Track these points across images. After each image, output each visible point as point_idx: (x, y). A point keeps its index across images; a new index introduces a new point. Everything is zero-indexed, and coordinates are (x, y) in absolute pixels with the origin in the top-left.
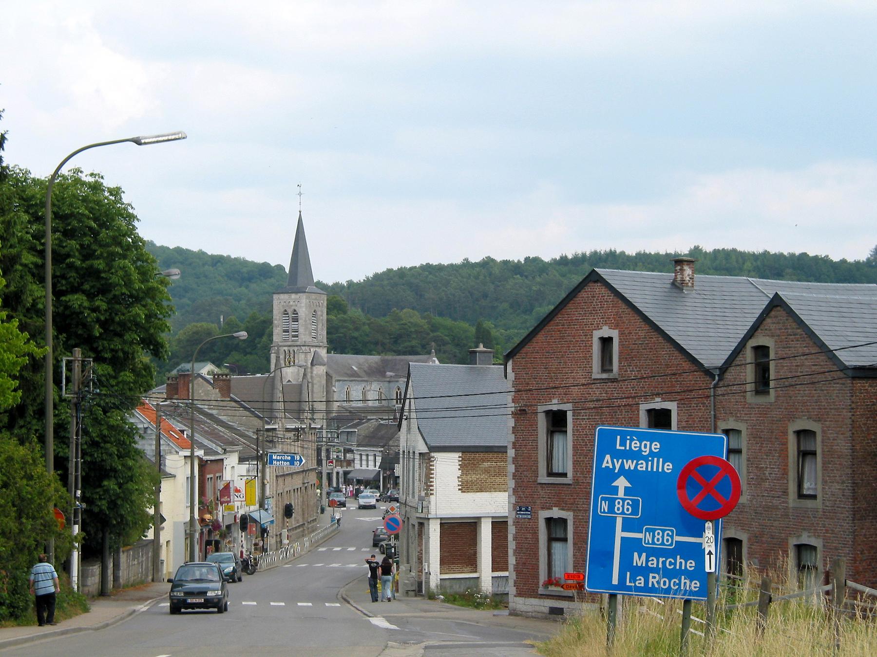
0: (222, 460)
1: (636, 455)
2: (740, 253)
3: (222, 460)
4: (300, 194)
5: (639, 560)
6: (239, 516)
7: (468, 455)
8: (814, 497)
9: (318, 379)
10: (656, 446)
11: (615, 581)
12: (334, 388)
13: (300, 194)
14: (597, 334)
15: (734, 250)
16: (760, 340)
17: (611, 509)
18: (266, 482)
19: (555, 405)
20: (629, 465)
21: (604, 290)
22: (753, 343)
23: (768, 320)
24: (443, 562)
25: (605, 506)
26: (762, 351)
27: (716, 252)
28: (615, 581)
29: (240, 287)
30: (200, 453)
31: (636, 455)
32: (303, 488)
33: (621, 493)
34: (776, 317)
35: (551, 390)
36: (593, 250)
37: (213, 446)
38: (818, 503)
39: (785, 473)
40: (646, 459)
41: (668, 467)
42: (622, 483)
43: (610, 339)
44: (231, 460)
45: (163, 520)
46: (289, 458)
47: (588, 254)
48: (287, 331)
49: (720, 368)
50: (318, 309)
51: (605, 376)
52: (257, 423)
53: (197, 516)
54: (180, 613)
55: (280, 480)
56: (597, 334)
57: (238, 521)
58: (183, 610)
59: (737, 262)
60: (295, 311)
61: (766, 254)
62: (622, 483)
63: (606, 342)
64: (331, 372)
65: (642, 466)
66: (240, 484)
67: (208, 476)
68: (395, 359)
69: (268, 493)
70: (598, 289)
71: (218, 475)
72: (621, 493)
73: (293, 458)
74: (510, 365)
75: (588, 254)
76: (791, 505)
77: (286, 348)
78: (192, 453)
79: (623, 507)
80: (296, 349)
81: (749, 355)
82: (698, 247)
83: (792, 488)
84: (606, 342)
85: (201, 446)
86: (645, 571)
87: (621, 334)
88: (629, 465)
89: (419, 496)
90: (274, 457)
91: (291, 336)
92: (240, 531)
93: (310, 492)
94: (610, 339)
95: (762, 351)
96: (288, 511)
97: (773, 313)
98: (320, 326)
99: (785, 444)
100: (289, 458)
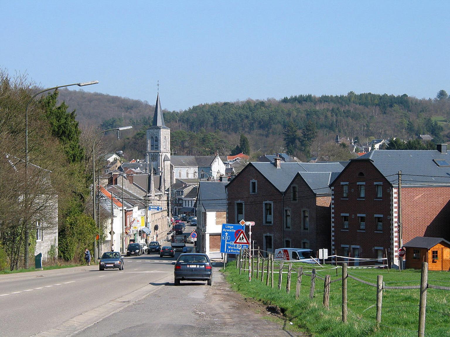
0: (132, 210)
1: (229, 229)
2: (373, 95)
3: (132, 210)
4: (158, 85)
5: (229, 247)
6: (138, 231)
7: (218, 213)
8: (307, 229)
9: (166, 167)
10: (233, 227)
11: (225, 251)
12: (173, 171)
13: (158, 85)
14: (251, 181)
15: (370, 94)
16: (294, 185)
17: (225, 238)
18: (148, 217)
19: (239, 201)
20: (228, 230)
21: (253, 168)
22: (292, 186)
23: (296, 180)
24: (210, 248)
25: (224, 238)
26: (294, 188)
27: (361, 95)
28: (225, 251)
29: (127, 112)
30: (125, 208)
31: (229, 229)
32: (162, 218)
33: (226, 235)
34: (298, 179)
35: (238, 199)
36: (300, 95)
37: (129, 205)
38: (308, 231)
39: (300, 222)
40: (231, 229)
41: (235, 231)
42: (227, 234)
43: (255, 183)
44: (136, 209)
45: (114, 233)
46: (157, 208)
47: (298, 96)
48: (153, 146)
49: (284, 192)
50: (166, 136)
51: (253, 193)
52: (144, 194)
53: (124, 232)
54: (103, 270)
55: (153, 215)
56: (251, 181)
57: (138, 232)
58: (105, 269)
59: (371, 100)
60: (156, 137)
61: (385, 96)
62: (227, 234)
63: (254, 184)
64: (172, 164)
65: (230, 231)
66: (139, 219)
67: (128, 216)
68: (201, 157)
69: (148, 221)
70: (251, 168)
71: (131, 215)
72: (226, 235)
73: (158, 207)
74: (227, 189)
75: (298, 96)
76: (302, 231)
77: (152, 153)
78: (123, 209)
79: (227, 238)
80: (157, 154)
81: (292, 188)
82: (352, 92)
83: (302, 226)
84: (254, 184)
85: (126, 205)
86: (230, 249)
87: (258, 181)
88: (228, 230)
89: (203, 226)
90: (151, 207)
91: (154, 148)
92: (139, 236)
93: (164, 219)
94: (255, 183)
95: (294, 188)
96: (156, 228)
97: (297, 178)
98: (167, 143)
99: (300, 214)
100: (157, 208)
